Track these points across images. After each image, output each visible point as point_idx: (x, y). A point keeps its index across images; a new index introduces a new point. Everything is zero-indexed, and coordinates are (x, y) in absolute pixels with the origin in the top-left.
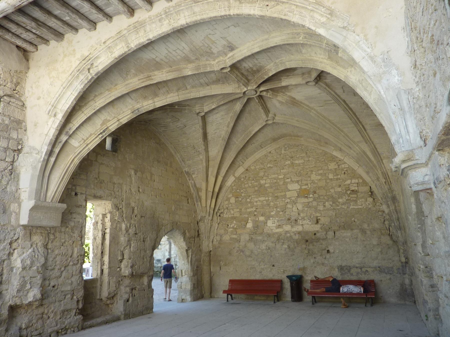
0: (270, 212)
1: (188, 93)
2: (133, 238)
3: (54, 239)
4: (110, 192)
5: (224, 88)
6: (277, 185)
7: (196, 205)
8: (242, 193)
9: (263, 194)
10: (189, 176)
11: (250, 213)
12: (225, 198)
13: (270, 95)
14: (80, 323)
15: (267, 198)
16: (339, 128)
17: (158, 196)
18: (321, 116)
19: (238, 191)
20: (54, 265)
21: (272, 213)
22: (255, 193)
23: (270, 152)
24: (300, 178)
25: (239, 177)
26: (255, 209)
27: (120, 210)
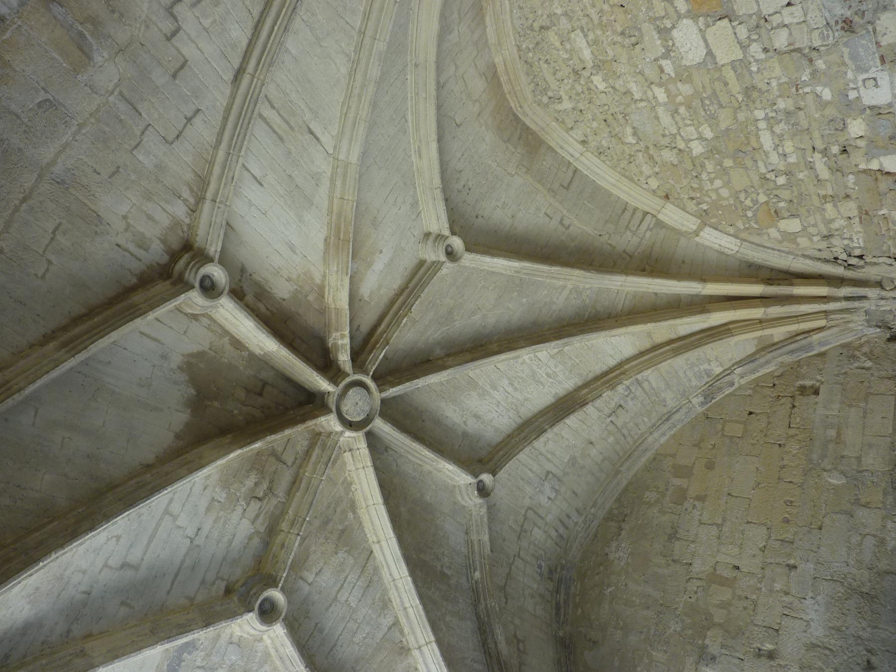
0: (823, 105)
1: (407, 616)
5: (366, 500)
6: (696, 103)
7: (823, 349)
8: (755, 202)
9: (747, 138)
10: (720, 389)
11: (836, 170)
12: (786, 246)
13: (342, 337)
15: (762, 125)
16: (367, 16)
17: (789, 555)
18: (351, 115)
19: (750, 214)
21: (827, 94)
22: (749, 163)
23: (584, 142)
24: (647, 27)
25: (700, 217)
26: (817, 156)
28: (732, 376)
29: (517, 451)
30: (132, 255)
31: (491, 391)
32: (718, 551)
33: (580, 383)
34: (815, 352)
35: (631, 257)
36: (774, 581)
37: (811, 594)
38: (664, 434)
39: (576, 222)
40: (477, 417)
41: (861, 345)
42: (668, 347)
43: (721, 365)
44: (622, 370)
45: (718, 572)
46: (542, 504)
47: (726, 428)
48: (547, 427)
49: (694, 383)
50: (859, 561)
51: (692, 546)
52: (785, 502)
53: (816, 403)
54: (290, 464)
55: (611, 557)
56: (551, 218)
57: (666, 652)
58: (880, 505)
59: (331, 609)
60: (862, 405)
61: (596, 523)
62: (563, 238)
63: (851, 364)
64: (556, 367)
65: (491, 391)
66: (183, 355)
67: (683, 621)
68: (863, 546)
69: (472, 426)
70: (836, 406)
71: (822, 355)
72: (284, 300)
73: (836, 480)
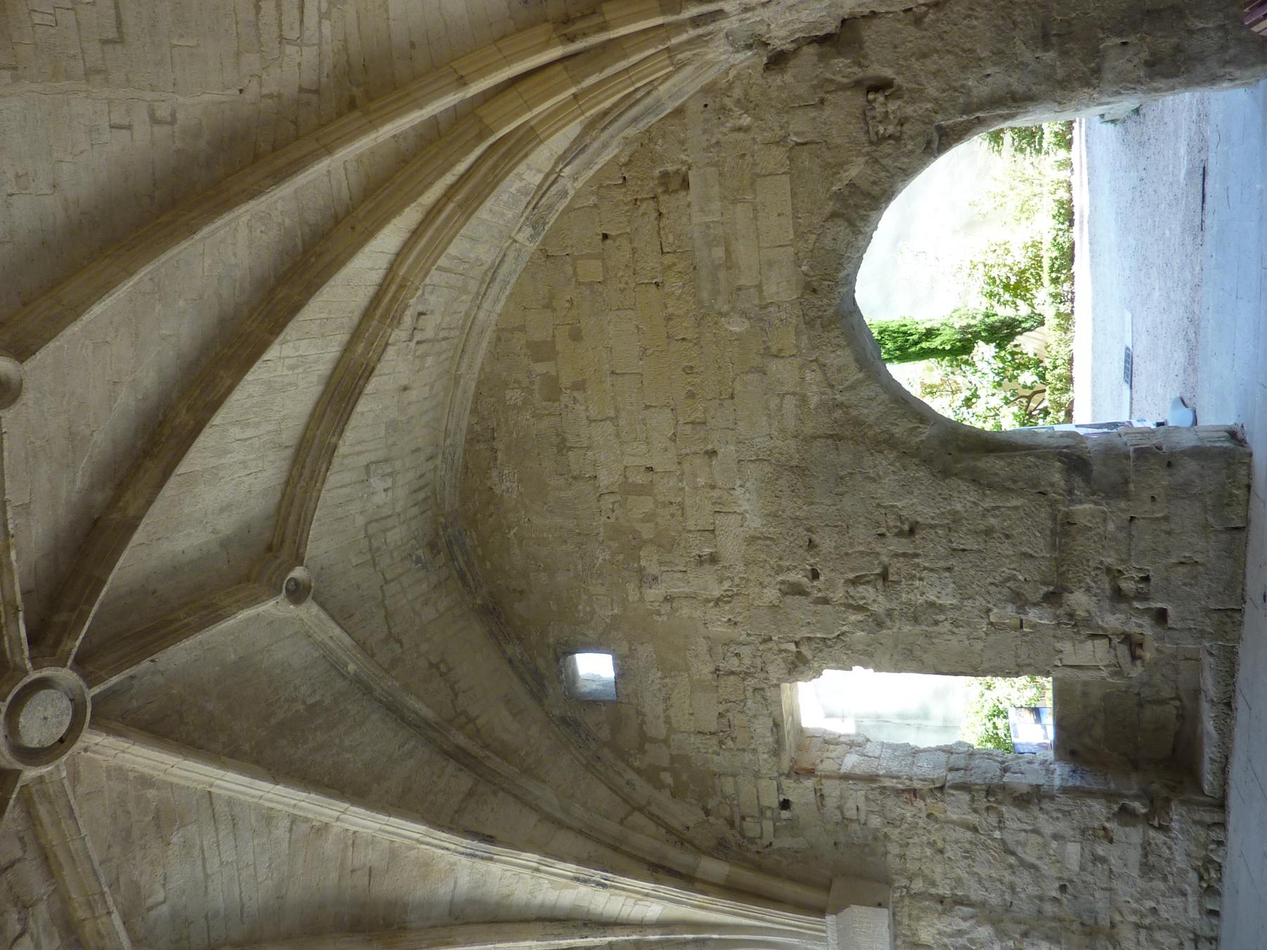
2: (904, 597)
3: (925, 877)
7: (677, 104)
10: (550, 207)
14: (1197, 817)
28: (561, 182)
29: (312, 505)
31: (223, 461)
32: (622, 454)
33: (346, 337)
34: (669, 110)
35: (317, 92)
36: (695, 476)
37: (739, 482)
38: (497, 300)
39: (181, 100)
41: (730, 85)
42: (451, 206)
43: (539, 171)
44: (398, 281)
45: (630, 480)
46: (381, 503)
47: (579, 271)
48: (334, 440)
49: (510, 215)
50: (782, 431)
51: (590, 453)
52: (684, 370)
53: (689, 205)
54: (19, 854)
55: (498, 491)
56: (129, 127)
58: (794, 352)
59: (210, 889)
60: (749, 197)
61: (460, 451)
62: (179, 145)
63: (723, 124)
64: (297, 349)
65: (223, 461)
67: (609, 547)
68: (784, 411)
69: (226, 525)
70: (716, 205)
71: (679, 112)
73: (737, 326)
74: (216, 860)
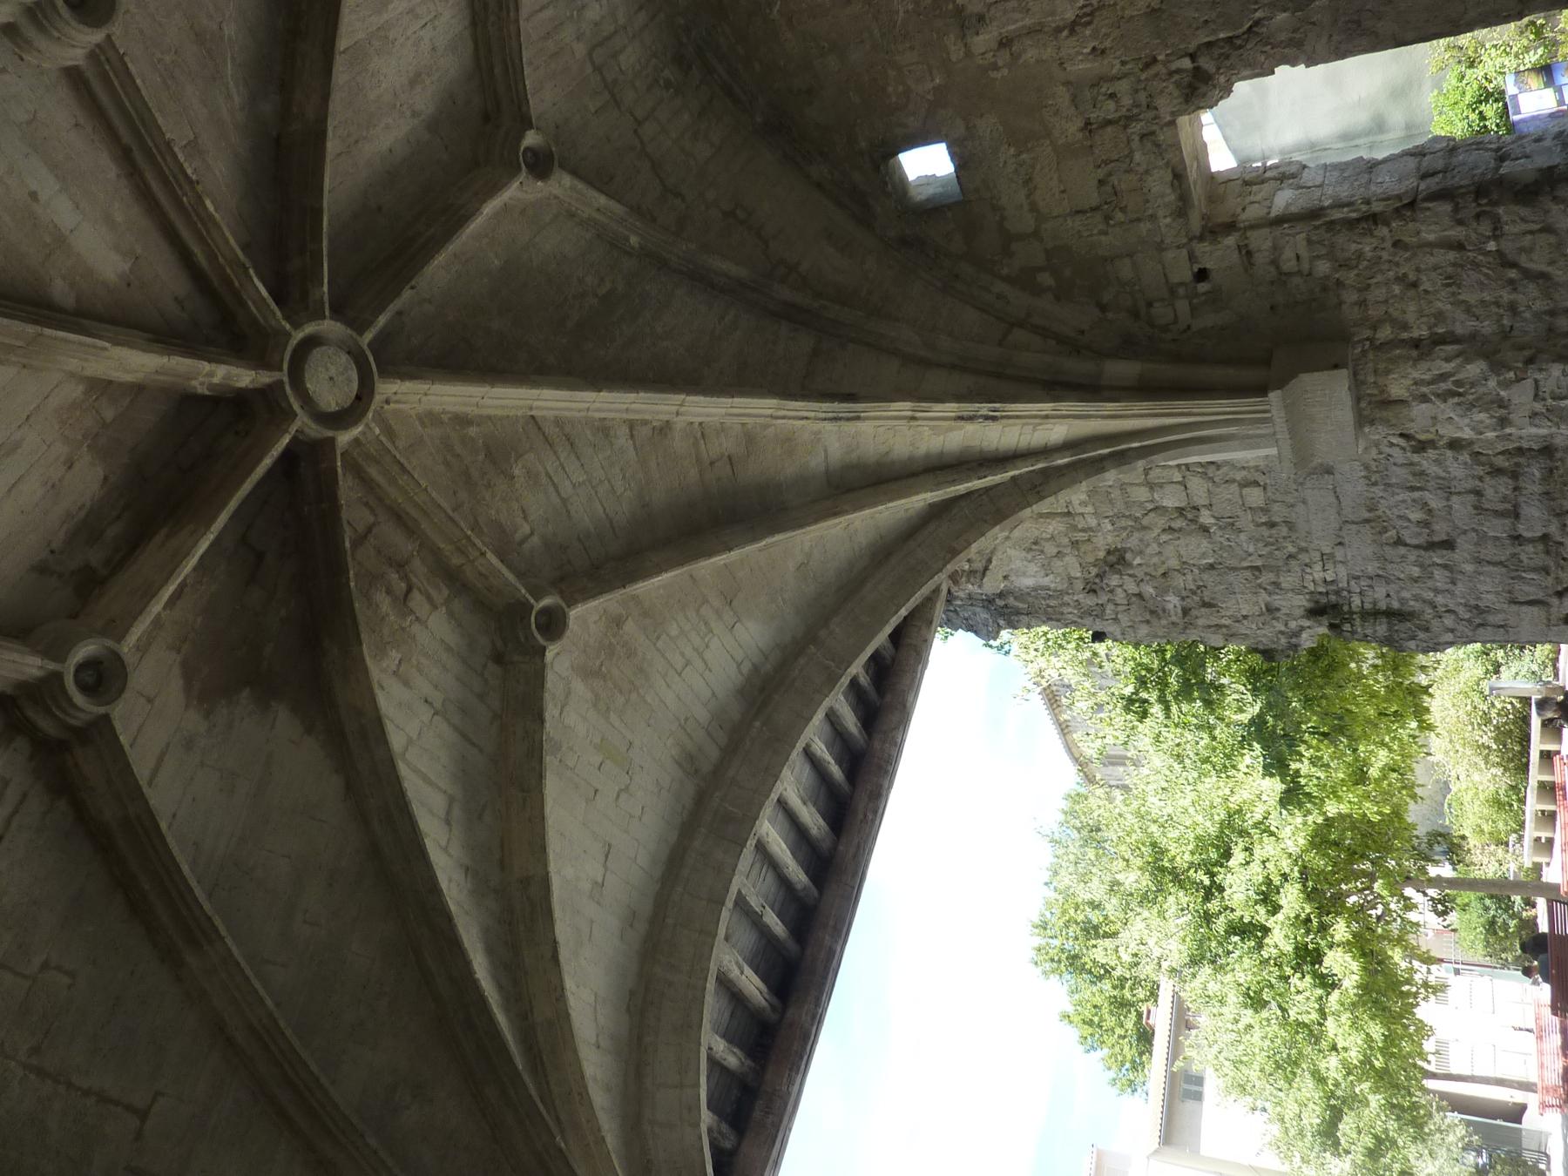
4: (1136, 144)
20: (1494, 309)
27: (1206, 63)
30: (15, 812)
31: (385, 17)
40: (414, 81)
54: (372, 519)
57: (912, 48)
59: (573, 513)
65: (385, 17)
66: (187, 706)
69: (424, 101)
72: (106, 478)
74: (567, 483)
